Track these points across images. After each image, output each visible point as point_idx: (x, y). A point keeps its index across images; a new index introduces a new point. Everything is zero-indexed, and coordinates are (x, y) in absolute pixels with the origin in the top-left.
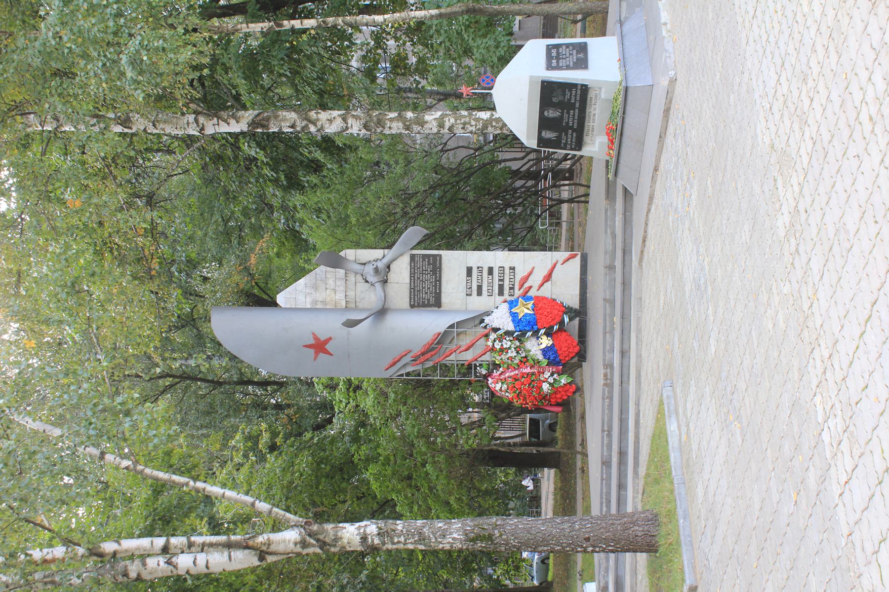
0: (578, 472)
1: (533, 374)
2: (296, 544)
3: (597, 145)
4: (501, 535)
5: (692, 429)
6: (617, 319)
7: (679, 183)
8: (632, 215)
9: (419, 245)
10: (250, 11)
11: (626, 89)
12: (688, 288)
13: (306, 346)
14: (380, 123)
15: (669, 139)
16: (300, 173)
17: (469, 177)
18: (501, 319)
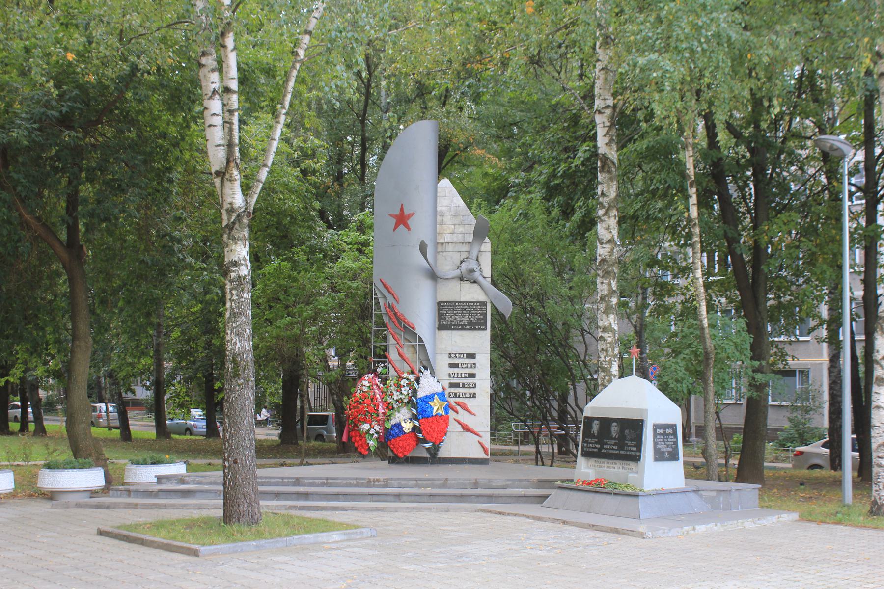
0: (282, 461)
1: (378, 415)
2: (231, 204)
3: (587, 470)
4: (239, 385)
5: (336, 552)
6: (429, 490)
7: (552, 541)
8: (524, 503)
9: (495, 309)
10: (711, 152)
11: (636, 496)
12: (459, 548)
13: (402, 206)
14: (607, 274)
15: (591, 533)
16: (561, 198)
17: (559, 355)
18: (428, 385)
